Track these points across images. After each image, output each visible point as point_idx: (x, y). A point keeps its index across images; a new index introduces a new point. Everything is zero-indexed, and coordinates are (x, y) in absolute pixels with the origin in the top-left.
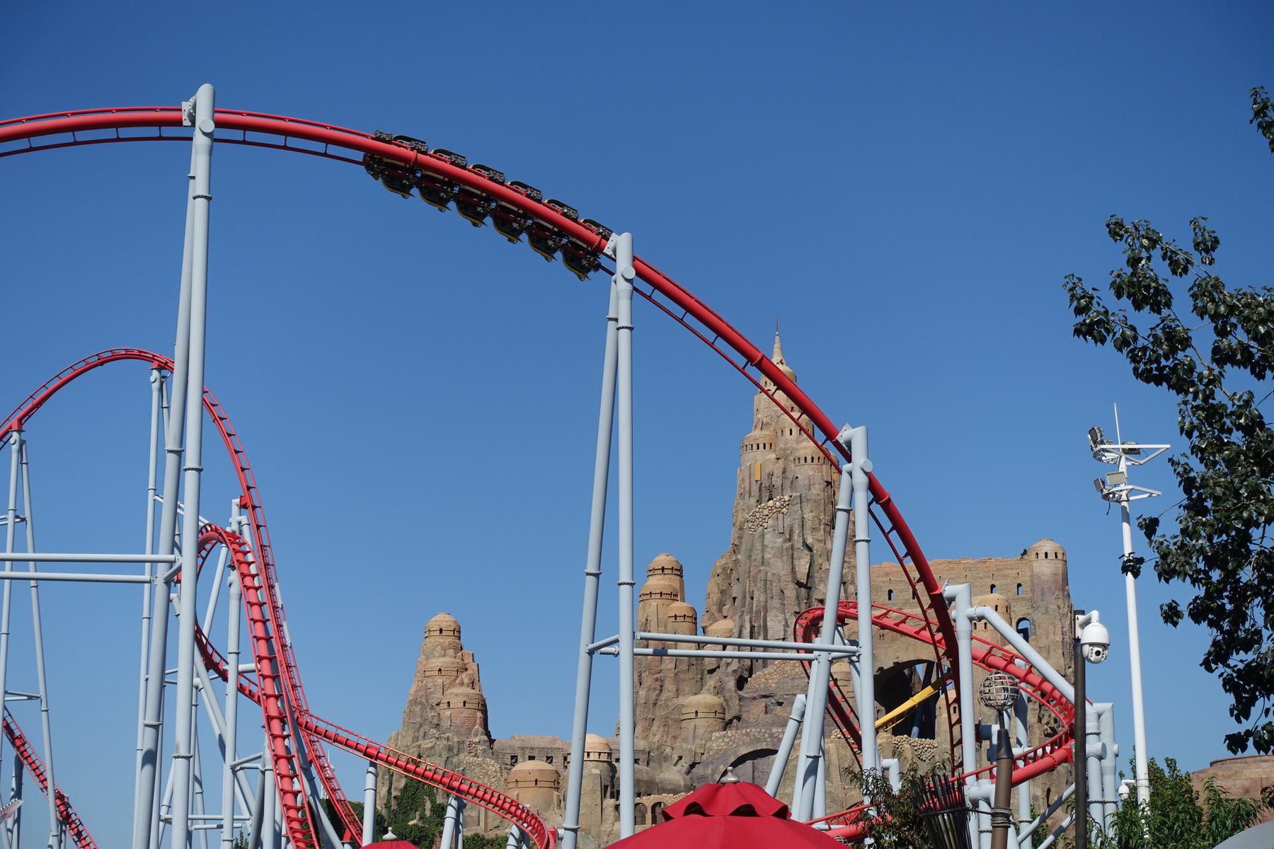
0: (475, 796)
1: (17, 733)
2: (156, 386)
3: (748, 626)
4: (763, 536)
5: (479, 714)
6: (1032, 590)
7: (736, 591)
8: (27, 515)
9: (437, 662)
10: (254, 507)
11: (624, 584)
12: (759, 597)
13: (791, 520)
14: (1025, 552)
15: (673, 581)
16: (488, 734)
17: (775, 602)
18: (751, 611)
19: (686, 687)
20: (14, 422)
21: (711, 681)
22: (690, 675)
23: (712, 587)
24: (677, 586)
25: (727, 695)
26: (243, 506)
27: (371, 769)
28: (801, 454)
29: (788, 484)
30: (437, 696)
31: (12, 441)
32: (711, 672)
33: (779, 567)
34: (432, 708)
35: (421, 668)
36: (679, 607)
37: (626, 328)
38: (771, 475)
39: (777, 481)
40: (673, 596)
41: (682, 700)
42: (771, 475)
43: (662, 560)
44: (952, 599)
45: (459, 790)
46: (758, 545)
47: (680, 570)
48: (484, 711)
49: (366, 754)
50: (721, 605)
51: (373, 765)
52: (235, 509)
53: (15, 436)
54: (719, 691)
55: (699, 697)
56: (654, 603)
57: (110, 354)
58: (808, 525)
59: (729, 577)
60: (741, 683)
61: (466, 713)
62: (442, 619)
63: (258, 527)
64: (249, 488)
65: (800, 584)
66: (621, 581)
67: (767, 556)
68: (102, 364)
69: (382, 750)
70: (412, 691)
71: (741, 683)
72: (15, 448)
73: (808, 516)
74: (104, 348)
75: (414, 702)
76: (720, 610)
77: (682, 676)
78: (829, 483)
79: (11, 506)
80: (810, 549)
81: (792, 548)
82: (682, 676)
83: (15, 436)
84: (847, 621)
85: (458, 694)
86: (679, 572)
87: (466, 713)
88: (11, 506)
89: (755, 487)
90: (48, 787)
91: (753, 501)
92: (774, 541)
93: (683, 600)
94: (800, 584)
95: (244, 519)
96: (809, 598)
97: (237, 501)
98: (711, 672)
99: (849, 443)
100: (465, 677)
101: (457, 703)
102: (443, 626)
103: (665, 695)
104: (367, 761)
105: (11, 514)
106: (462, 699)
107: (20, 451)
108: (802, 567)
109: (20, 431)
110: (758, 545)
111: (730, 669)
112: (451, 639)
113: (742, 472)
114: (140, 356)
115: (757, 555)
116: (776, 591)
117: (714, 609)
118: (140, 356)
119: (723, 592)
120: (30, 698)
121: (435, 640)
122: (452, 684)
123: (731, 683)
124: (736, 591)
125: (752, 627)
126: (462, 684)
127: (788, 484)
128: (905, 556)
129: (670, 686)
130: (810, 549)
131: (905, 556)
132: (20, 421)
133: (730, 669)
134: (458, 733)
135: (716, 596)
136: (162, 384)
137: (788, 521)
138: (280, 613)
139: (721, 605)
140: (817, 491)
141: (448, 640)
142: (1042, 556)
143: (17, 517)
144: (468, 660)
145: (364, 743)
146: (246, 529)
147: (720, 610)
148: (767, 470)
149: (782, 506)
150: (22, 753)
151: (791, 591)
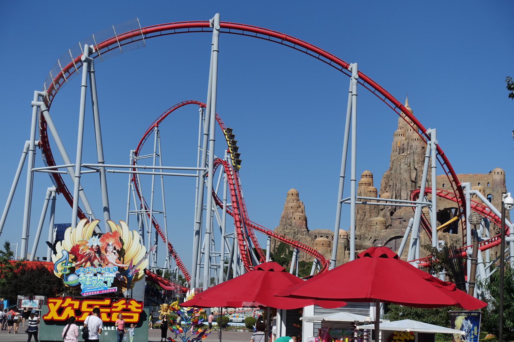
1: (156, 224)
2: (201, 113)
3: (394, 195)
4: (400, 165)
5: (304, 222)
6: (493, 185)
7: (391, 183)
8: (160, 154)
9: (291, 204)
12: (399, 185)
15: (370, 180)
16: (307, 228)
17: (404, 187)
18: (396, 190)
20: (156, 124)
21: (382, 213)
24: (371, 181)
27: (269, 239)
28: (414, 138)
29: (409, 148)
30: (290, 216)
31: (155, 130)
32: (382, 210)
33: (406, 175)
34: (289, 219)
35: (286, 206)
36: (371, 188)
37: (355, 95)
38: (403, 145)
39: (405, 147)
40: (369, 184)
41: (372, 219)
42: (403, 145)
43: (366, 172)
44: (464, 187)
45: (297, 246)
46: (399, 168)
47: (372, 176)
48: (306, 221)
49: (267, 234)
50: (386, 188)
52: (226, 153)
53: (156, 128)
54: (384, 216)
55: (378, 218)
56: (363, 187)
58: (416, 161)
60: (392, 214)
61: (300, 221)
62: (292, 190)
65: (412, 181)
67: (402, 172)
68: (183, 105)
69: (272, 233)
70: (283, 214)
71: (392, 214)
72: (156, 132)
73: (416, 158)
75: (283, 217)
76: (385, 190)
77: (372, 211)
80: (416, 170)
82: (372, 211)
83: (156, 128)
84: (428, 194)
85: (298, 215)
87: (300, 221)
88: (155, 151)
89: (398, 149)
91: (397, 153)
92: (404, 167)
94: (412, 181)
96: (415, 186)
97: (227, 150)
98: (382, 210)
99: (430, 134)
100: (300, 209)
101: (297, 218)
102: (293, 193)
103: (366, 217)
104: (267, 236)
105: (155, 154)
107: (158, 133)
108: (414, 176)
109: (157, 127)
110: (399, 168)
111: (388, 209)
112: (296, 197)
114: (196, 103)
115: (398, 171)
116: (404, 184)
117: (383, 189)
118: (196, 103)
119: (386, 183)
120: (160, 213)
121: (290, 197)
122: (296, 212)
123: (388, 214)
124: (391, 183)
125: (396, 195)
126: (299, 212)
127: (409, 148)
128: (448, 173)
129: (368, 214)
130: (416, 170)
131: (448, 173)
132: (157, 123)
133: (388, 209)
134: (297, 228)
135: (384, 185)
136: (203, 112)
137: (409, 160)
139: (386, 188)
140: (419, 150)
143: (156, 154)
144: (301, 204)
147: (385, 190)
148: (402, 143)
149: (407, 155)
150: (158, 230)
151: (409, 183)
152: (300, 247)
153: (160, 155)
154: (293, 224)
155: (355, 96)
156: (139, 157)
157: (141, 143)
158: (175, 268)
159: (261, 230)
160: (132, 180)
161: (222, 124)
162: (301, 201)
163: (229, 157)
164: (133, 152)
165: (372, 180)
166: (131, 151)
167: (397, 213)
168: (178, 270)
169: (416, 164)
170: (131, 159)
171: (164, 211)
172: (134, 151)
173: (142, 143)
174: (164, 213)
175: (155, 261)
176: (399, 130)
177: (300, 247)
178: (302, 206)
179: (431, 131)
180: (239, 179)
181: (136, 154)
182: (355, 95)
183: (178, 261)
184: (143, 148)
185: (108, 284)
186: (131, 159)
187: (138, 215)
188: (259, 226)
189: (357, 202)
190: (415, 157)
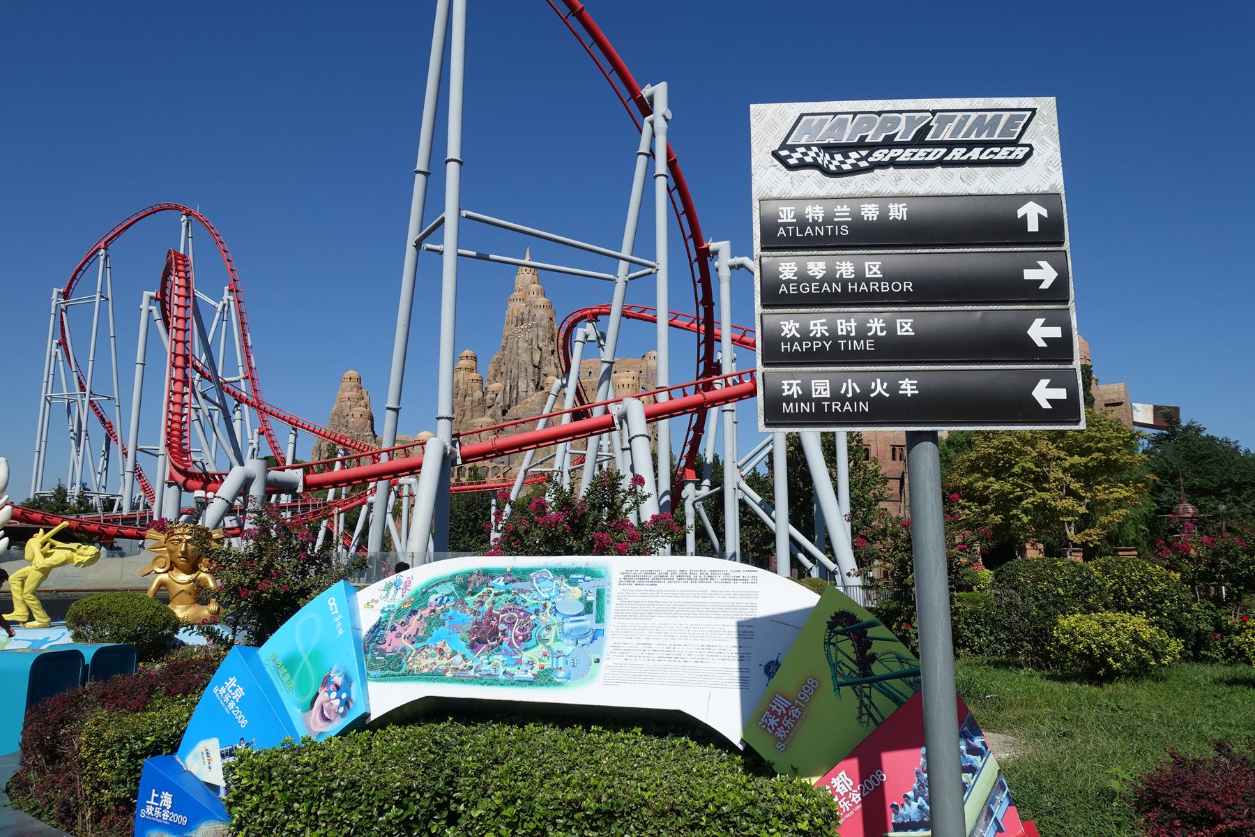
0: (354, 448)
1: (107, 420)
2: (184, 224)
3: (509, 385)
4: (517, 342)
5: (369, 421)
6: (647, 374)
7: (503, 369)
8: (109, 296)
9: (348, 394)
10: (237, 291)
11: (443, 418)
12: (515, 371)
13: (529, 336)
14: (644, 356)
15: (472, 363)
16: (374, 432)
17: (523, 374)
18: (510, 379)
19: (476, 415)
20: (102, 244)
21: (489, 412)
22: (479, 409)
23: (491, 369)
24: (474, 365)
25: (497, 418)
26: (231, 291)
27: (293, 432)
28: (538, 304)
29: (531, 318)
30: (347, 411)
31: (100, 254)
32: (489, 407)
33: (525, 357)
34: (344, 417)
35: (339, 397)
36: (474, 375)
37: (446, 418)
38: (522, 314)
39: (525, 316)
40: (472, 370)
41: (474, 421)
42: (522, 314)
43: (467, 352)
44: (716, 253)
45: (345, 444)
46: (515, 347)
47: (476, 358)
48: (372, 420)
49: (289, 422)
50: (495, 377)
51: (294, 429)
52: (226, 292)
53: (102, 251)
54: (493, 416)
55: (483, 419)
56: (462, 373)
57: (159, 207)
58: (540, 338)
59: (500, 362)
60: (504, 412)
61: (362, 420)
62: (352, 373)
63: (239, 302)
64: (234, 280)
65: (535, 366)
66: (449, 157)
67: (519, 352)
68: (154, 212)
69: (300, 421)
70: (334, 409)
71: (504, 412)
72: (102, 258)
73: (540, 333)
74: (155, 202)
75: (335, 414)
76: (494, 379)
77: (474, 409)
78: (551, 319)
79: (99, 290)
80: (541, 350)
81: (532, 348)
82: (474, 409)
83: (102, 251)
84: (599, 318)
85: (358, 410)
86: (475, 359)
87: (362, 420)
88: (99, 290)
89: (515, 320)
90: (129, 454)
91: (513, 326)
92: (523, 345)
93: (476, 372)
94: (535, 366)
95: (231, 298)
96: (539, 373)
97: (228, 287)
98: (489, 407)
99: (651, 98)
100: (362, 402)
101: (357, 415)
102: (352, 376)
103: (466, 418)
104: (290, 427)
105: (98, 295)
106: (360, 413)
107: (106, 259)
108: (537, 358)
109: (105, 249)
110: (515, 347)
111: (499, 406)
112: (356, 383)
113: (509, 312)
114: (176, 208)
115: (514, 351)
116: (523, 369)
117: (492, 379)
118: (176, 208)
119: (496, 370)
120: (109, 398)
121: (347, 383)
122: (355, 405)
123: (500, 412)
124: (503, 369)
125: (511, 386)
126: (360, 406)
127: (531, 318)
128: (682, 214)
129: (468, 414)
130: (541, 350)
131: (682, 214)
132: (106, 243)
133: (499, 406)
134: (357, 430)
135: (493, 372)
136: (188, 224)
137: (530, 336)
138: (250, 350)
139: (495, 377)
140: (545, 321)
141: (354, 383)
142: (652, 358)
143: (102, 297)
144: (364, 394)
145: (288, 417)
146: (232, 303)
147: (494, 379)
148: (521, 311)
149: (528, 328)
150: (109, 431)
151: (531, 369)
152: (350, 446)
153: (110, 299)
154: (351, 425)
155: (447, 420)
156: (73, 300)
157: (74, 277)
158: (137, 495)
159: (277, 417)
160: (60, 344)
161: (221, 242)
162: (364, 391)
163: (231, 298)
164: (59, 293)
165: (476, 364)
166: (55, 291)
167: (513, 411)
168: (142, 499)
169: (540, 341)
170: (54, 304)
171: (116, 396)
172: (62, 290)
173: (78, 277)
174: (117, 399)
175: (104, 484)
176: (516, 293)
177: (354, 448)
178: (367, 398)
179: (659, 93)
180: (248, 335)
181: (66, 295)
182: (446, 418)
183: (144, 483)
184: (79, 286)
185: (942, 613)
186: (54, 304)
187: (69, 403)
188: (274, 409)
189: (460, 251)
190: (540, 331)
